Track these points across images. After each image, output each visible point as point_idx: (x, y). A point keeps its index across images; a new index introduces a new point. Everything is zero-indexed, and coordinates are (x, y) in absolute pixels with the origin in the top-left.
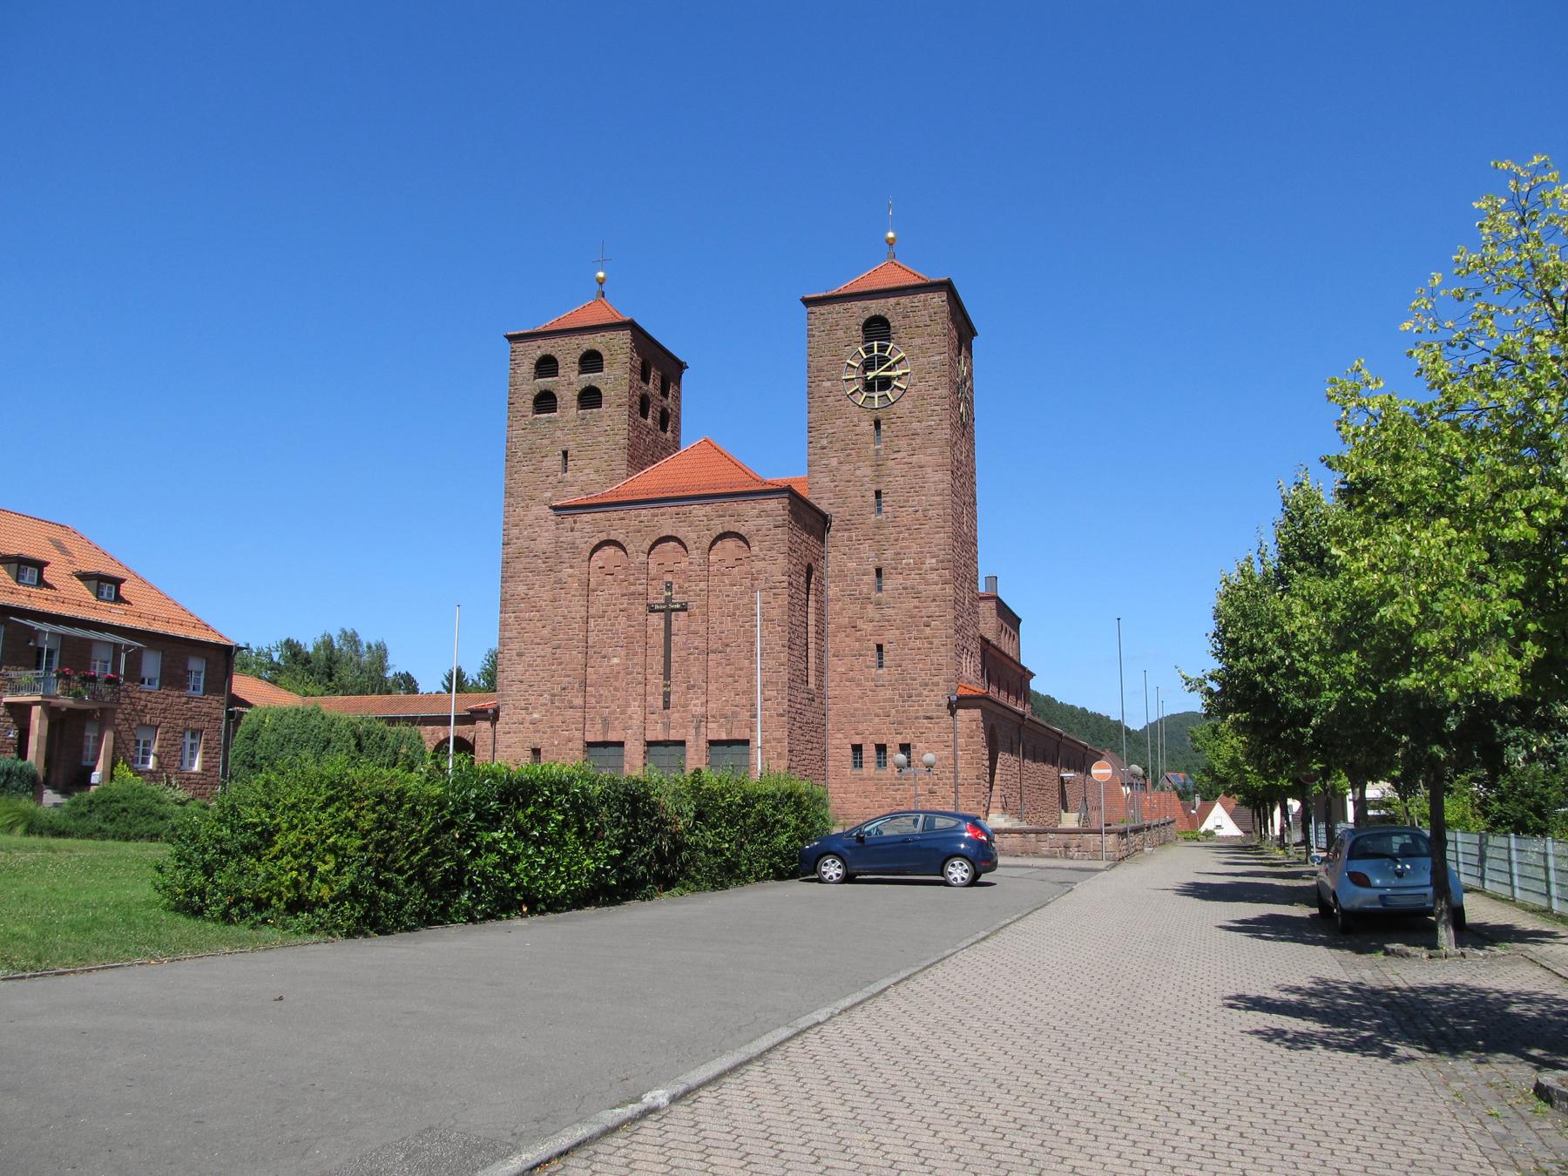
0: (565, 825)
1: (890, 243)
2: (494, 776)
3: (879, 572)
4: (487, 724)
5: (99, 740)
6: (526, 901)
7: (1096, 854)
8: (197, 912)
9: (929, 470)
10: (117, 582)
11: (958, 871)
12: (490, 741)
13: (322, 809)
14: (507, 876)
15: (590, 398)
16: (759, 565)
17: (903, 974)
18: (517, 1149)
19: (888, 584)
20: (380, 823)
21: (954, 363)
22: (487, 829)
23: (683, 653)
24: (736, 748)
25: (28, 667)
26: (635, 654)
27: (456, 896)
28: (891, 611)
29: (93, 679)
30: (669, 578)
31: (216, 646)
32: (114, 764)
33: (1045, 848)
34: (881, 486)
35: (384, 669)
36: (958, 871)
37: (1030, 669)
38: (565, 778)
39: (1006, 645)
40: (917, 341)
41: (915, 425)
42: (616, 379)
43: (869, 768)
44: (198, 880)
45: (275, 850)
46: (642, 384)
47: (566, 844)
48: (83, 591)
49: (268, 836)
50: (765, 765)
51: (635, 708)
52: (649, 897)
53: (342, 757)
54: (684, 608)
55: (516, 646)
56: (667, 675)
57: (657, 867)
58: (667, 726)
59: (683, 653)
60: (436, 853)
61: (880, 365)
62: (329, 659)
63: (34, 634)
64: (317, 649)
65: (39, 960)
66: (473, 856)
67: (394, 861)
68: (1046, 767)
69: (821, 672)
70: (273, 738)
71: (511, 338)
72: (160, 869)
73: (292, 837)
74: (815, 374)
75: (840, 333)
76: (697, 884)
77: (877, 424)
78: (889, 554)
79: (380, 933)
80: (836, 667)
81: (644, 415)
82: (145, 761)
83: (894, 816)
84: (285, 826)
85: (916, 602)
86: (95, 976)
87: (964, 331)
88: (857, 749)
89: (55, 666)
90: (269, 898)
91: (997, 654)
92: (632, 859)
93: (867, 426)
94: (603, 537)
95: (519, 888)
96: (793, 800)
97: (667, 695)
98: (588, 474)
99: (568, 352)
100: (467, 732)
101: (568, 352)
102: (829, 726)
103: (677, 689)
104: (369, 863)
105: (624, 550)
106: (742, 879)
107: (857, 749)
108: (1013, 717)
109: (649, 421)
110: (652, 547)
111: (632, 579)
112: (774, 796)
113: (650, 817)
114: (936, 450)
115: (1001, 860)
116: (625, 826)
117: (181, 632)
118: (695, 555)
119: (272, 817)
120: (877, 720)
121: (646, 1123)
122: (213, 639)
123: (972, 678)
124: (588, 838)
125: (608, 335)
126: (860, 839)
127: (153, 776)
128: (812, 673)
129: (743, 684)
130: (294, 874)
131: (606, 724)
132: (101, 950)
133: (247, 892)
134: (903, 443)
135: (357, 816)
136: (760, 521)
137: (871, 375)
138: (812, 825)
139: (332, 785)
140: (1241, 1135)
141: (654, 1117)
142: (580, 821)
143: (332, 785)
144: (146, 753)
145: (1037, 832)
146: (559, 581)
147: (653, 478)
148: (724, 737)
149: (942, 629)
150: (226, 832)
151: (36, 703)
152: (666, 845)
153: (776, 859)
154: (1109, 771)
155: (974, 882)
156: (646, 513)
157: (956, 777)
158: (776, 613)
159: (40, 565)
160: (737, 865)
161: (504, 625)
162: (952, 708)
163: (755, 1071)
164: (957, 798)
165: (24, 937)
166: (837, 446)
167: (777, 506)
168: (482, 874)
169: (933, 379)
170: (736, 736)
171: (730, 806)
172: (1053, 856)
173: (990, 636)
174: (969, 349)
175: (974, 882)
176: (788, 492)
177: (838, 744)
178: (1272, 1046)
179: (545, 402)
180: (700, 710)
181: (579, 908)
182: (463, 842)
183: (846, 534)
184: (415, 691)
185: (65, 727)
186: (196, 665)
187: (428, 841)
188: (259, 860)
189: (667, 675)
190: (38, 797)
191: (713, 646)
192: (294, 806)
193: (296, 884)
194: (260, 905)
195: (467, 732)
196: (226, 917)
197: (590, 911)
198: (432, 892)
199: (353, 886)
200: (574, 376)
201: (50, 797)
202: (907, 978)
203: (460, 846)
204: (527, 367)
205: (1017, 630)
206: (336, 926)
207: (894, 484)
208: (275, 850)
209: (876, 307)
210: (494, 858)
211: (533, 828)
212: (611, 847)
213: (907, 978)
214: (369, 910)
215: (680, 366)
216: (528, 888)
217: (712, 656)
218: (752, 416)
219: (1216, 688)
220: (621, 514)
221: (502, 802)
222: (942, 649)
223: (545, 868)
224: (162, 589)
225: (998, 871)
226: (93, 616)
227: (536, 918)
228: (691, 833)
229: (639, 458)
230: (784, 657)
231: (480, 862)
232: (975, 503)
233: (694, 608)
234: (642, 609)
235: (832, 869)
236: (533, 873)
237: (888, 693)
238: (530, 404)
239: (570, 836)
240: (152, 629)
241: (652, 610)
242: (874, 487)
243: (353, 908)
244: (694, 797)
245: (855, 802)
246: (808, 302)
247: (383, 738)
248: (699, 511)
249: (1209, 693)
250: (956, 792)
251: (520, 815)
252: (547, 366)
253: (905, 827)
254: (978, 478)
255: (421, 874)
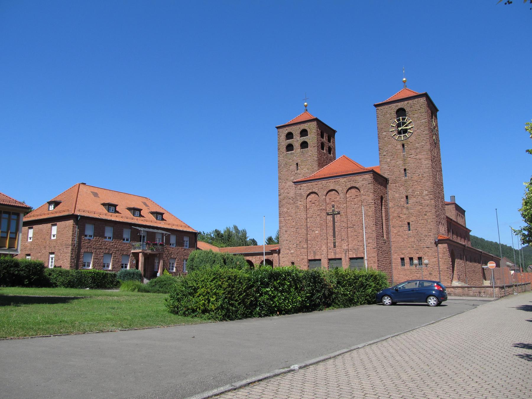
0: (290, 286)
1: (404, 82)
2: (267, 271)
3: (407, 197)
4: (276, 255)
5: (159, 263)
6: (278, 310)
7: (491, 295)
8: (177, 313)
9: (423, 160)
10: (162, 214)
11: (432, 301)
12: (278, 260)
13: (212, 281)
14: (272, 302)
15: (304, 145)
16: (364, 197)
17: (396, 334)
18: (246, 378)
19: (411, 201)
20: (229, 285)
21: (430, 122)
22: (265, 288)
23: (339, 229)
24: (359, 260)
25: (138, 241)
26: (323, 229)
27: (255, 309)
28: (412, 211)
29: (156, 244)
30: (333, 203)
31: (192, 233)
32: (163, 270)
33: (471, 293)
34: (406, 167)
35: (246, 238)
36: (432, 301)
37: (469, 228)
38: (290, 271)
39: (460, 221)
40: (416, 115)
41: (417, 145)
42: (312, 138)
43: (407, 266)
44: (176, 304)
45: (197, 294)
46: (321, 139)
47: (291, 292)
48: (152, 217)
49: (195, 290)
50: (370, 265)
51: (324, 247)
52: (320, 310)
53: (218, 266)
54: (339, 213)
55: (284, 229)
56: (334, 236)
57: (324, 300)
58: (335, 253)
59: (339, 229)
60: (247, 295)
61: (403, 125)
62: (229, 235)
63: (139, 231)
64: (225, 232)
65: (130, 325)
66: (260, 296)
67: (235, 297)
68: (476, 264)
69: (388, 233)
70: (198, 260)
71: (278, 128)
72: (166, 300)
73: (202, 290)
74: (380, 130)
75: (388, 115)
76: (339, 305)
77: (403, 145)
78: (410, 191)
79: (231, 320)
80: (393, 231)
81: (323, 149)
82: (173, 269)
83: (409, 282)
84: (200, 287)
85: (421, 207)
86: (146, 330)
87: (433, 110)
88: (402, 259)
89: (145, 241)
90: (197, 309)
91: (455, 224)
92: (314, 297)
93: (400, 147)
94: (311, 191)
95: (276, 306)
96: (375, 278)
97: (335, 243)
98: (305, 170)
99: (296, 130)
100: (270, 257)
101: (296, 130)
102: (392, 252)
103: (338, 241)
104: (226, 298)
105: (318, 195)
106: (355, 304)
107: (402, 259)
108: (461, 246)
109: (325, 151)
110: (327, 193)
111: (321, 204)
112: (366, 276)
113: (320, 283)
114: (425, 153)
115: (449, 297)
116: (311, 286)
117: (181, 229)
118: (342, 195)
119: (197, 284)
120: (409, 249)
121: (289, 374)
122: (191, 231)
123: (444, 233)
124: (299, 290)
125: (309, 124)
126: (397, 290)
127: (175, 274)
128: (385, 233)
129: (360, 238)
130: (203, 301)
131: (315, 253)
132: (147, 323)
133: (190, 307)
134: (413, 151)
135: (222, 283)
136: (363, 182)
137: (400, 129)
138: (381, 286)
139: (214, 274)
140: (493, 387)
141: (292, 372)
142: (296, 285)
143: (214, 274)
144: (173, 267)
145: (468, 287)
146: (297, 207)
147: (327, 170)
148: (355, 256)
149: (431, 216)
150: (184, 289)
151: (140, 252)
152: (327, 293)
153: (368, 297)
154: (495, 265)
155: (439, 304)
156: (324, 182)
157: (439, 268)
158: (370, 213)
159: (140, 210)
160: (353, 299)
161: (280, 222)
162: (436, 244)
163: (331, 361)
164: (440, 276)
165: (127, 319)
166: (390, 154)
167: (368, 177)
168: (263, 302)
169: (422, 128)
170: (359, 256)
171: (349, 279)
172: (475, 296)
173: (453, 218)
174: (436, 116)
175: (439, 304)
176: (372, 172)
177: (396, 258)
178: (523, 360)
179: (290, 147)
180: (346, 248)
181: (297, 313)
182: (257, 291)
183: (394, 185)
184: (256, 244)
185: (149, 259)
186: (186, 239)
187: (245, 291)
188: (194, 297)
189: (334, 236)
190: (142, 281)
191: (350, 225)
192: (203, 280)
193: (204, 304)
194: (194, 311)
195: (270, 257)
196: (184, 314)
197: (300, 314)
198: (247, 307)
199: (221, 305)
200: (298, 138)
201: (146, 281)
202: (397, 335)
203: (258, 291)
204: (283, 136)
205: (464, 215)
206: (217, 318)
207: (411, 165)
208: (197, 294)
209: (400, 105)
210: (267, 296)
211: (280, 287)
212: (307, 293)
213: (397, 335)
214: (227, 313)
215: (334, 132)
216: (279, 306)
217: (349, 229)
218: (359, 147)
219: (526, 233)
220: (316, 183)
221: (269, 279)
222: (432, 223)
223: (284, 300)
224: (175, 216)
225: (447, 301)
226: (155, 225)
227: (282, 316)
228: (335, 288)
229: (322, 163)
230: (374, 228)
231: (262, 298)
232: (441, 171)
233: (342, 213)
234: (325, 214)
235: (387, 300)
236: (280, 302)
237: (413, 239)
238: (285, 149)
239: (292, 290)
240: (172, 228)
241: (328, 214)
242: (404, 168)
243: (222, 312)
244: (336, 277)
245: (401, 277)
246: (376, 106)
247: (232, 260)
248: (342, 180)
249: (524, 235)
250: (440, 274)
251: (275, 283)
252: (290, 136)
253: (412, 286)
254: (442, 162)
255: (243, 301)
